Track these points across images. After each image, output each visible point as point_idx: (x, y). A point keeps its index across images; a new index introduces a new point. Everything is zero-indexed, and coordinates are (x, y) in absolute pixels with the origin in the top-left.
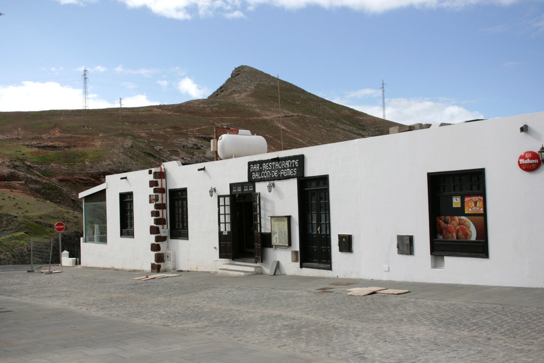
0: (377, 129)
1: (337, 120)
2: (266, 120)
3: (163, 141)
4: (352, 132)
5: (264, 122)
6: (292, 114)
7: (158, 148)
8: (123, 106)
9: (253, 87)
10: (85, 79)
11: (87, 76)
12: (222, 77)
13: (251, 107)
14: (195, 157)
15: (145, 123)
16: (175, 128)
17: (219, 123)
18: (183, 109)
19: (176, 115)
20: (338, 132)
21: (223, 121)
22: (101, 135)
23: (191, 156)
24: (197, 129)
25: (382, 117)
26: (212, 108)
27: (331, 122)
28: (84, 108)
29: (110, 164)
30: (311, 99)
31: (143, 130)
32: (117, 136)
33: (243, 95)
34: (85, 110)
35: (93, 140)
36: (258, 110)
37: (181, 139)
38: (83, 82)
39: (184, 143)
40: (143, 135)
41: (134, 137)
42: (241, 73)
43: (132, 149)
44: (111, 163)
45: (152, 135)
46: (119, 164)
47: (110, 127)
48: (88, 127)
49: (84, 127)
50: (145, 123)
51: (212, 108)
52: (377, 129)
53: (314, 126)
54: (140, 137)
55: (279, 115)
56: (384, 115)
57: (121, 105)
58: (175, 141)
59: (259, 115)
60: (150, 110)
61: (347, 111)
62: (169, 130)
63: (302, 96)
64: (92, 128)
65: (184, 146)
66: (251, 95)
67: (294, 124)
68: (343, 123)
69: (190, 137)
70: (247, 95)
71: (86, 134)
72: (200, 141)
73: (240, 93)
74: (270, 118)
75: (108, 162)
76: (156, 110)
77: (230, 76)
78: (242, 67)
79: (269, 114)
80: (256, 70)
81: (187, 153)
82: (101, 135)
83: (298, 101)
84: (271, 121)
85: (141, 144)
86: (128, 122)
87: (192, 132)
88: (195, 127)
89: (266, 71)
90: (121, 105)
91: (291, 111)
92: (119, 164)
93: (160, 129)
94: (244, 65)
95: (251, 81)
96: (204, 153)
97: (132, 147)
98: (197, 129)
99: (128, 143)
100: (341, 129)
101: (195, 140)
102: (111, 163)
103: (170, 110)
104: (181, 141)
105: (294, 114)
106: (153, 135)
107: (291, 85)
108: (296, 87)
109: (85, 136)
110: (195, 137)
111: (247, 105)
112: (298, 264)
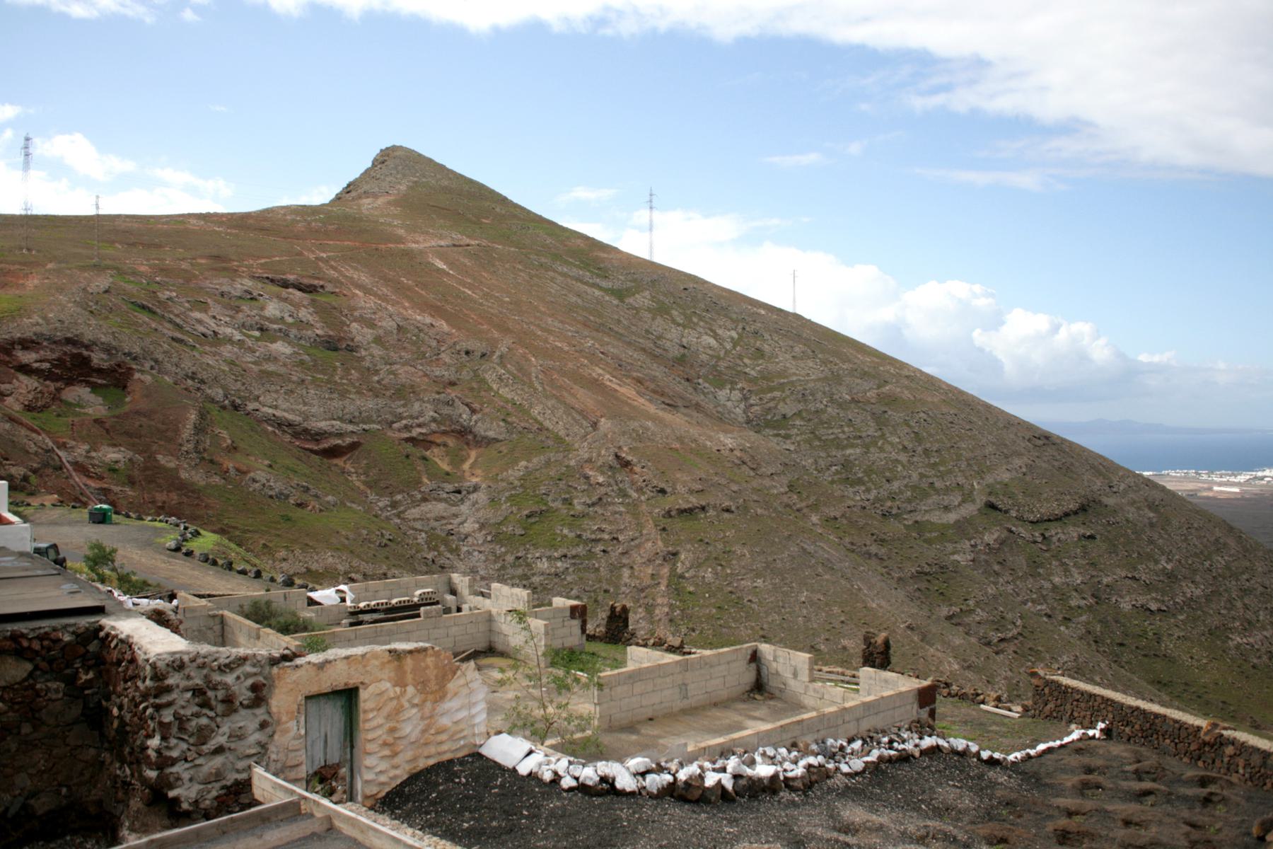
0: (629, 277)
1: (556, 257)
2: (412, 250)
3: (181, 281)
4: (581, 281)
5: (408, 254)
6: (468, 241)
7: (164, 295)
8: (101, 212)
9: (403, 188)
10: (27, 155)
11: (31, 150)
12: (357, 164)
13: (390, 224)
14: (240, 315)
15: (159, 246)
16: (217, 258)
17: (313, 252)
18: (251, 221)
19: (230, 234)
20: (552, 279)
21: (322, 248)
22: (50, 266)
23: (232, 313)
24: (263, 261)
25: (647, 257)
26: (309, 223)
27: (543, 260)
28: (23, 213)
29: (38, 324)
30: (515, 216)
31: (148, 260)
32: (83, 269)
33: (381, 201)
34: (26, 216)
35: (26, 276)
36: (401, 232)
37: (221, 280)
38: (22, 158)
39: (225, 288)
40: (143, 269)
41: (120, 272)
42: (393, 160)
43: (106, 296)
44: (40, 321)
45: (162, 270)
46: (58, 325)
47: (80, 250)
48: (29, 250)
49: (21, 249)
50: (159, 246)
51: (309, 223)
52: (629, 277)
53: (507, 266)
54: (134, 273)
55: (442, 243)
56: (651, 252)
57: (98, 208)
58: (207, 283)
59: (400, 240)
60: (183, 222)
61: (579, 241)
62: (203, 261)
63: (498, 210)
64: (38, 251)
65: (222, 295)
66: (396, 203)
67: (466, 261)
68: (566, 263)
69: (240, 276)
70: (389, 203)
71: (20, 263)
72: (260, 285)
73: (375, 196)
74: (422, 246)
75: (36, 318)
76: (194, 221)
77: (369, 165)
78: (394, 148)
79: (421, 239)
80: (420, 155)
81: (225, 307)
82: (50, 266)
83: (487, 218)
84: (421, 252)
85: (129, 287)
86: (120, 243)
87: (249, 267)
88: (259, 258)
89: (439, 160)
90: (98, 208)
91: (468, 237)
92: (58, 325)
93: (183, 259)
94: (398, 144)
95: (404, 175)
96: (262, 309)
97: (106, 292)
98: (263, 261)
99: (103, 282)
100: (560, 274)
101: (249, 283)
102: (40, 321)
103: (221, 224)
104: (222, 283)
105: (473, 242)
106: (164, 270)
107: (481, 187)
108: (492, 192)
109: (17, 267)
110: (253, 277)
111: (382, 220)
112: (89, 553)
